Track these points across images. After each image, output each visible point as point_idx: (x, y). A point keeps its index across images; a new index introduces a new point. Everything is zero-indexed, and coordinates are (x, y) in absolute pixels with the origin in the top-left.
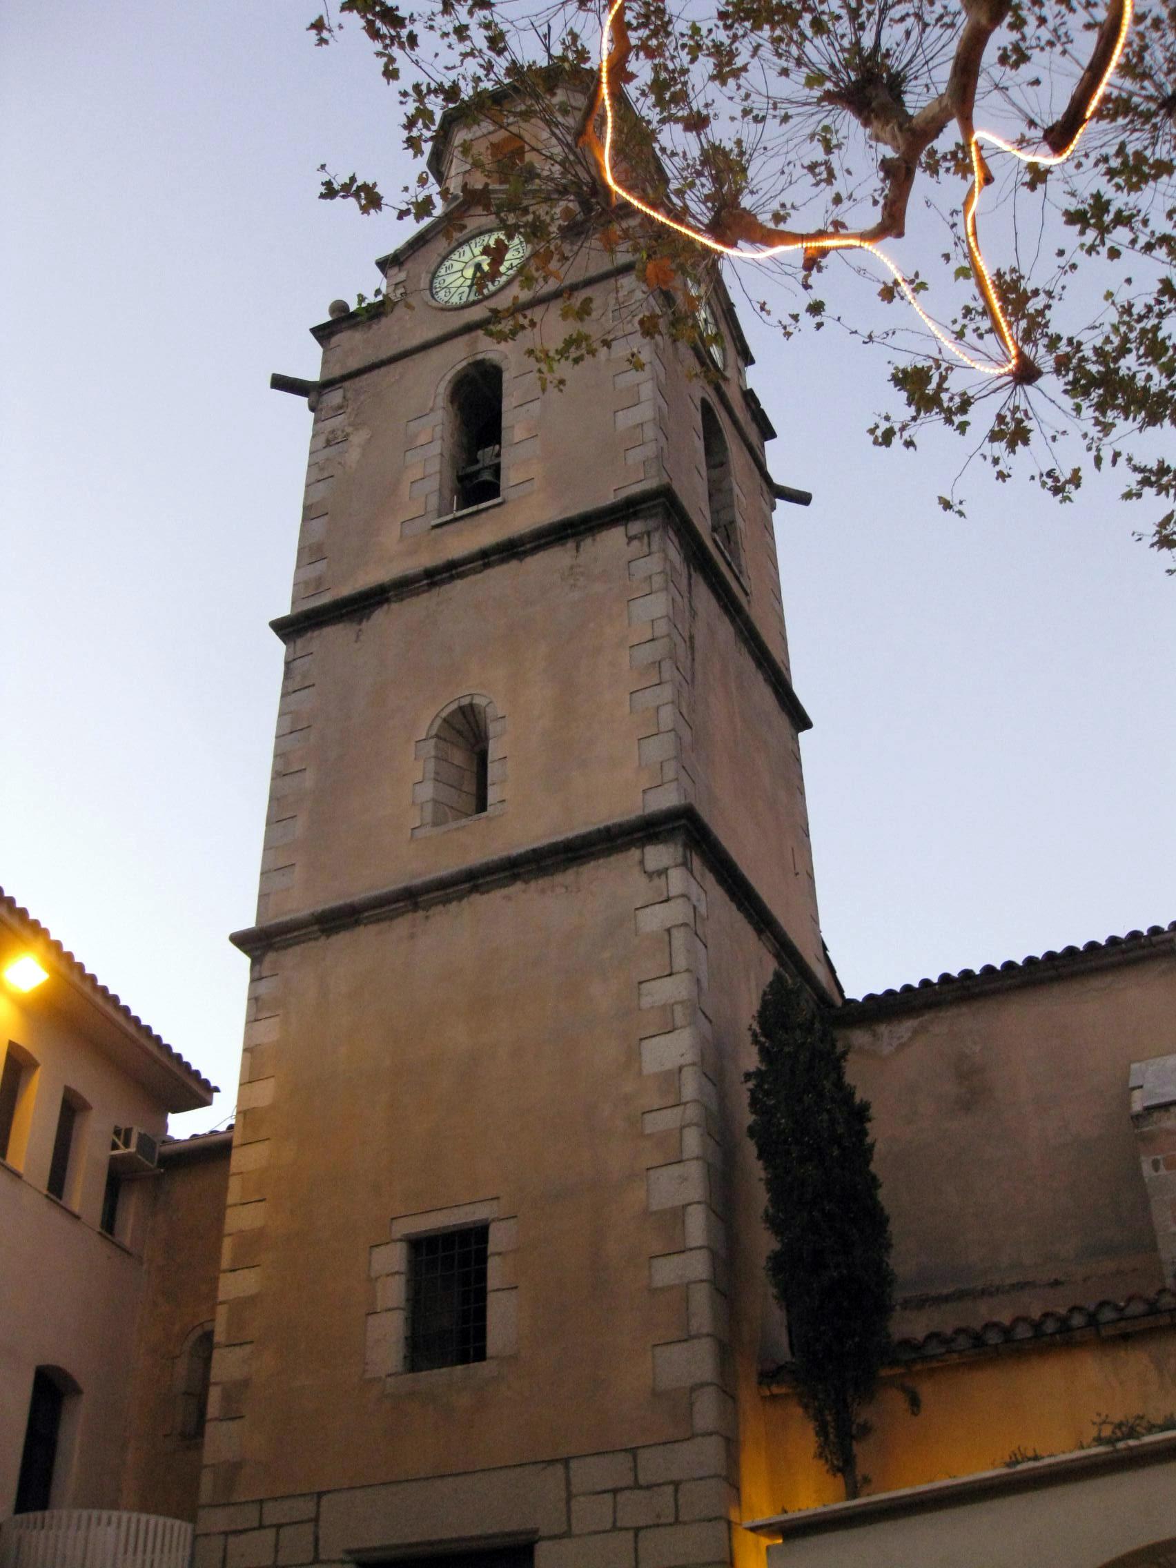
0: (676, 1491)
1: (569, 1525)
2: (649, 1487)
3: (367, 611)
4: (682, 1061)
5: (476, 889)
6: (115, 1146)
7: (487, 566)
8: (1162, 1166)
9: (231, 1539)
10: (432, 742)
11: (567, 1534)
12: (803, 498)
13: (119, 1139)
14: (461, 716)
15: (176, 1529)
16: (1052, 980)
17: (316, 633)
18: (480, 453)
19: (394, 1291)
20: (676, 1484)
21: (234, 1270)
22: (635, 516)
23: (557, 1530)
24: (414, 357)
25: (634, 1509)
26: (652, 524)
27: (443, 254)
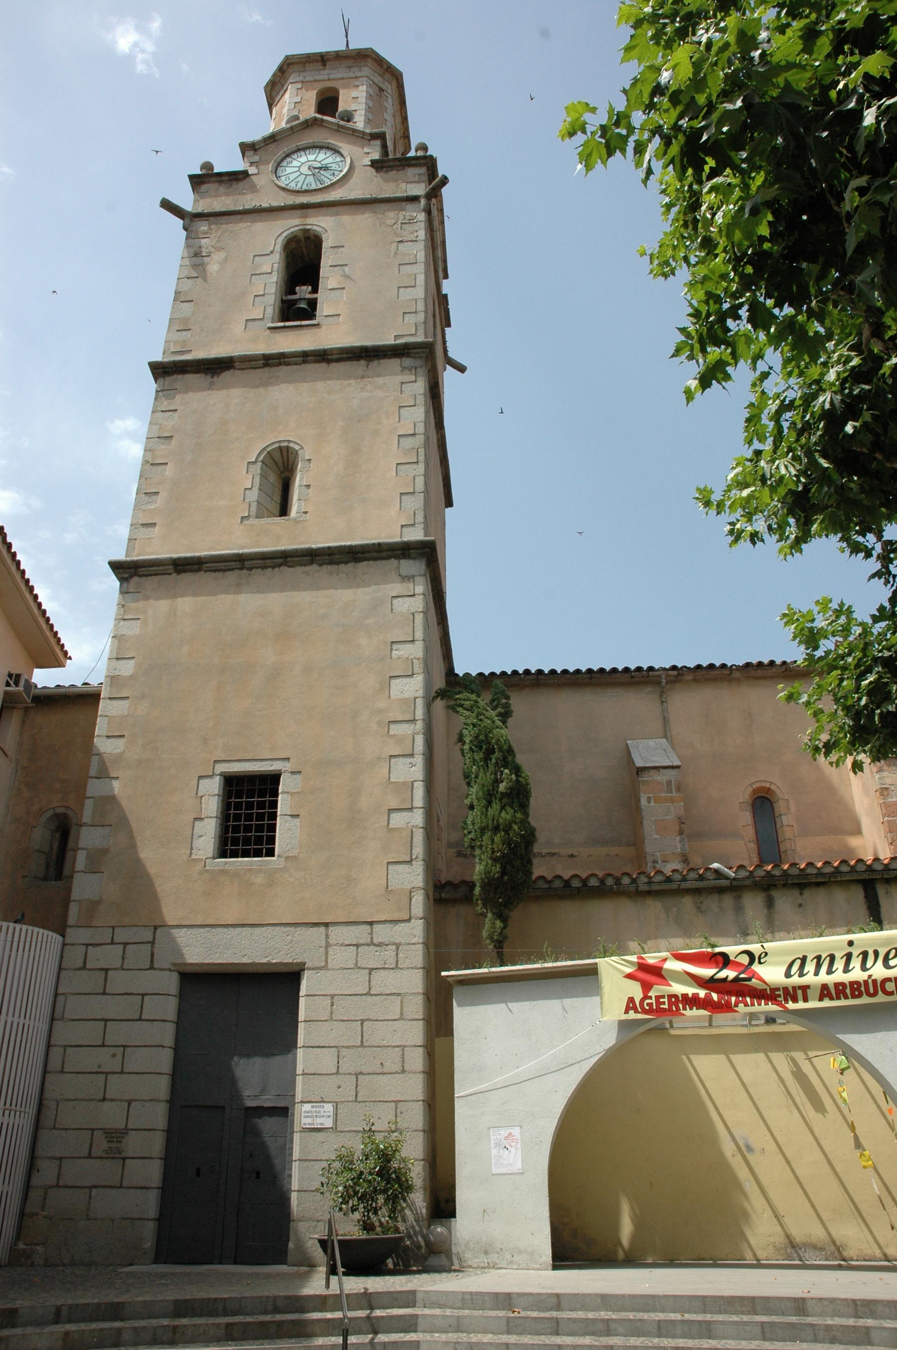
0: (397, 949)
1: (327, 962)
2: (380, 945)
3: (219, 371)
4: (417, 695)
5: (285, 564)
6: (8, 684)
7: (304, 362)
8: (652, 801)
9: (90, 947)
10: (259, 464)
11: (325, 967)
12: (462, 369)
13: (11, 680)
14: (279, 452)
15: (54, 938)
16: (587, 685)
17: (180, 376)
18: (297, 288)
19: (212, 806)
20: (398, 945)
21: (99, 778)
22: (408, 355)
23: (318, 964)
24: (262, 214)
25: (368, 956)
26: (419, 362)
27: (287, 153)
